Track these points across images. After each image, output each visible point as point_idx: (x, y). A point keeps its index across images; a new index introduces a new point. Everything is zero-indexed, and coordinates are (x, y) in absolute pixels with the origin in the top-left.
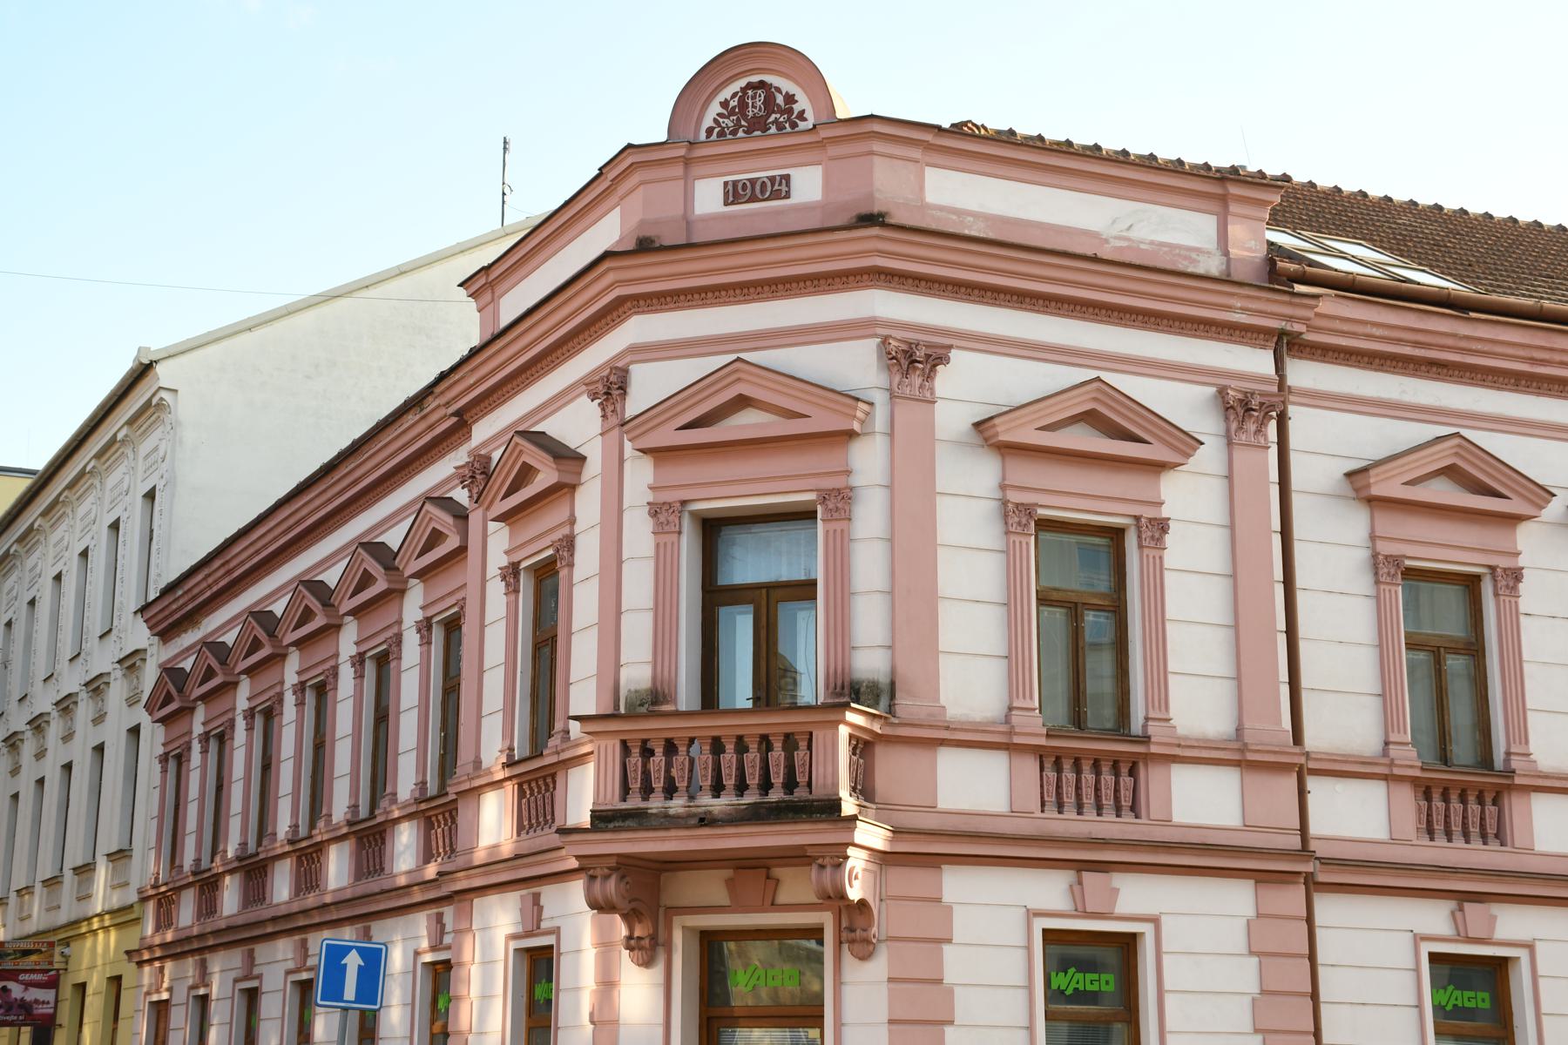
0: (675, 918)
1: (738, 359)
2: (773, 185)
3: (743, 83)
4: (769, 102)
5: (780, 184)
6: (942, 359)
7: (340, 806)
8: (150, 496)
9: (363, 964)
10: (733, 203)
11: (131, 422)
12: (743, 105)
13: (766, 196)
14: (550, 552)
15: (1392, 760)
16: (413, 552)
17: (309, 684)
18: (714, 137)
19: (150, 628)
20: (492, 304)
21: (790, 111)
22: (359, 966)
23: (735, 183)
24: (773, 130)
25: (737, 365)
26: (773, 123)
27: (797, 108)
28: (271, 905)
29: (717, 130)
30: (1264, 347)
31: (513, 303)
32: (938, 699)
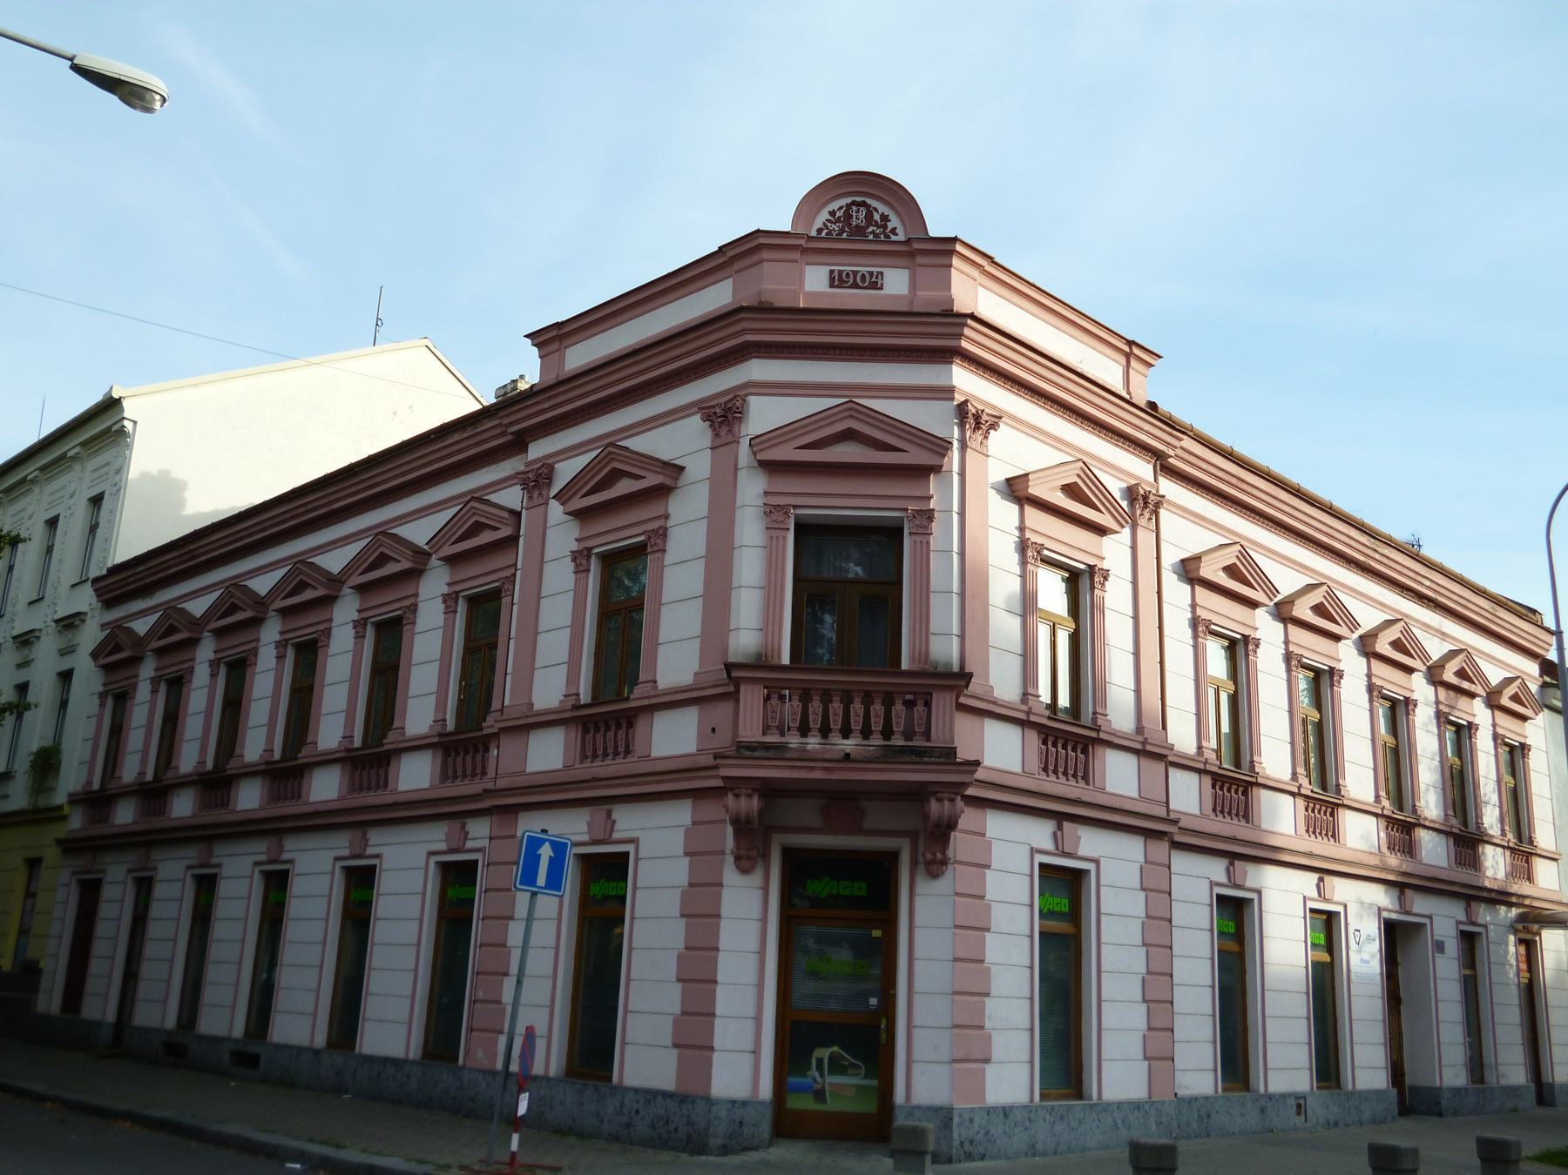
0: (774, 836)
1: (851, 401)
2: (871, 277)
3: (849, 200)
4: (869, 216)
5: (877, 277)
6: (994, 426)
7: (255, 745)
8: (97, 501)
9: (552, 855)
10: (837, 287)
11: (84, 444)
12: (848, 216)
13: (866, 284)
14: (642, 538)
15: (1206, 759)
16: (450, 538)
17: (291, 642)
18: (823, 235)
19: (98, 596)
20: (558, 353)
21: (885, 227)
22: (550, 857)
23: (840, 272)
24: (871, 237)
25: (851, 405)
26: (871, 233)
27: (890, 225)
28: (234, 811)
29: (825, 231)
30: (1149, 462)
31: (579, 356)
32: (988, 681)
